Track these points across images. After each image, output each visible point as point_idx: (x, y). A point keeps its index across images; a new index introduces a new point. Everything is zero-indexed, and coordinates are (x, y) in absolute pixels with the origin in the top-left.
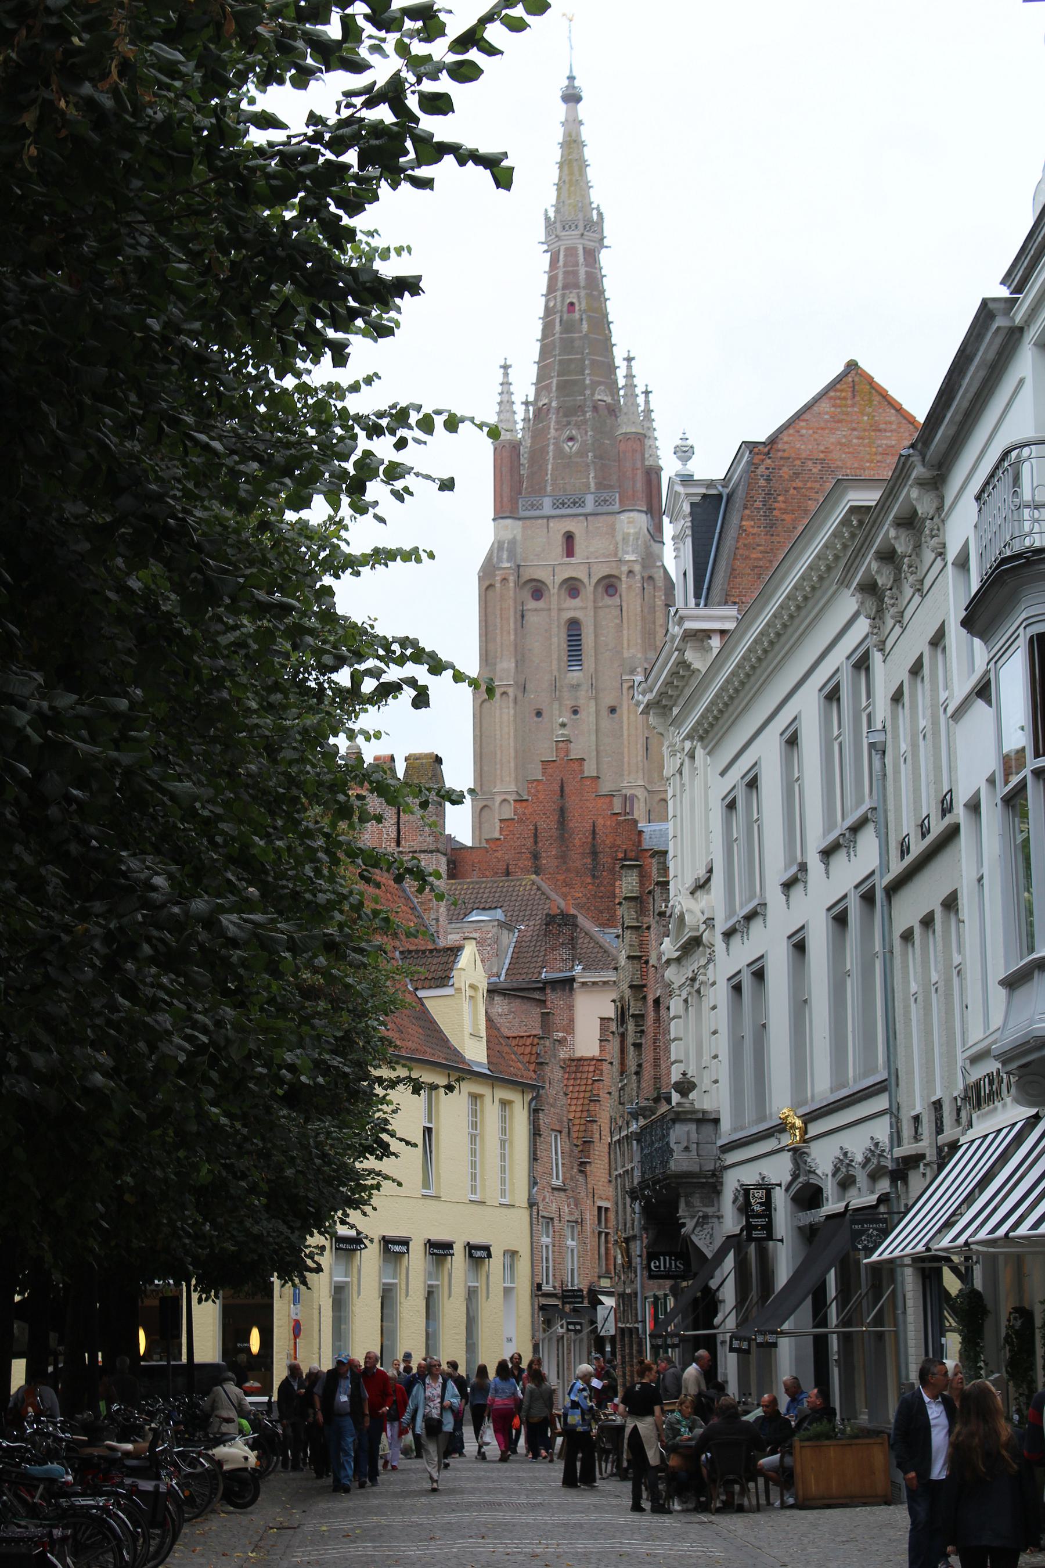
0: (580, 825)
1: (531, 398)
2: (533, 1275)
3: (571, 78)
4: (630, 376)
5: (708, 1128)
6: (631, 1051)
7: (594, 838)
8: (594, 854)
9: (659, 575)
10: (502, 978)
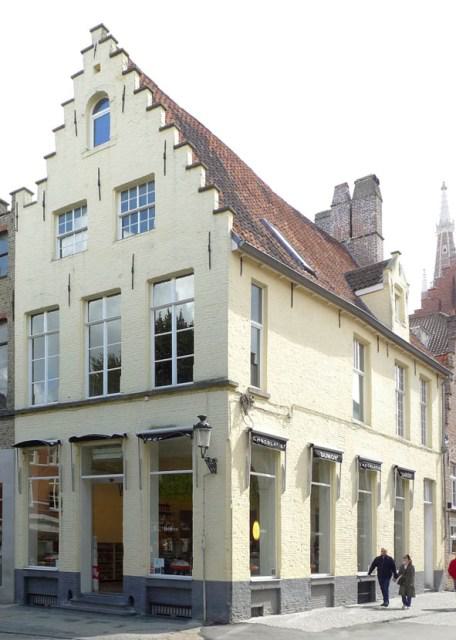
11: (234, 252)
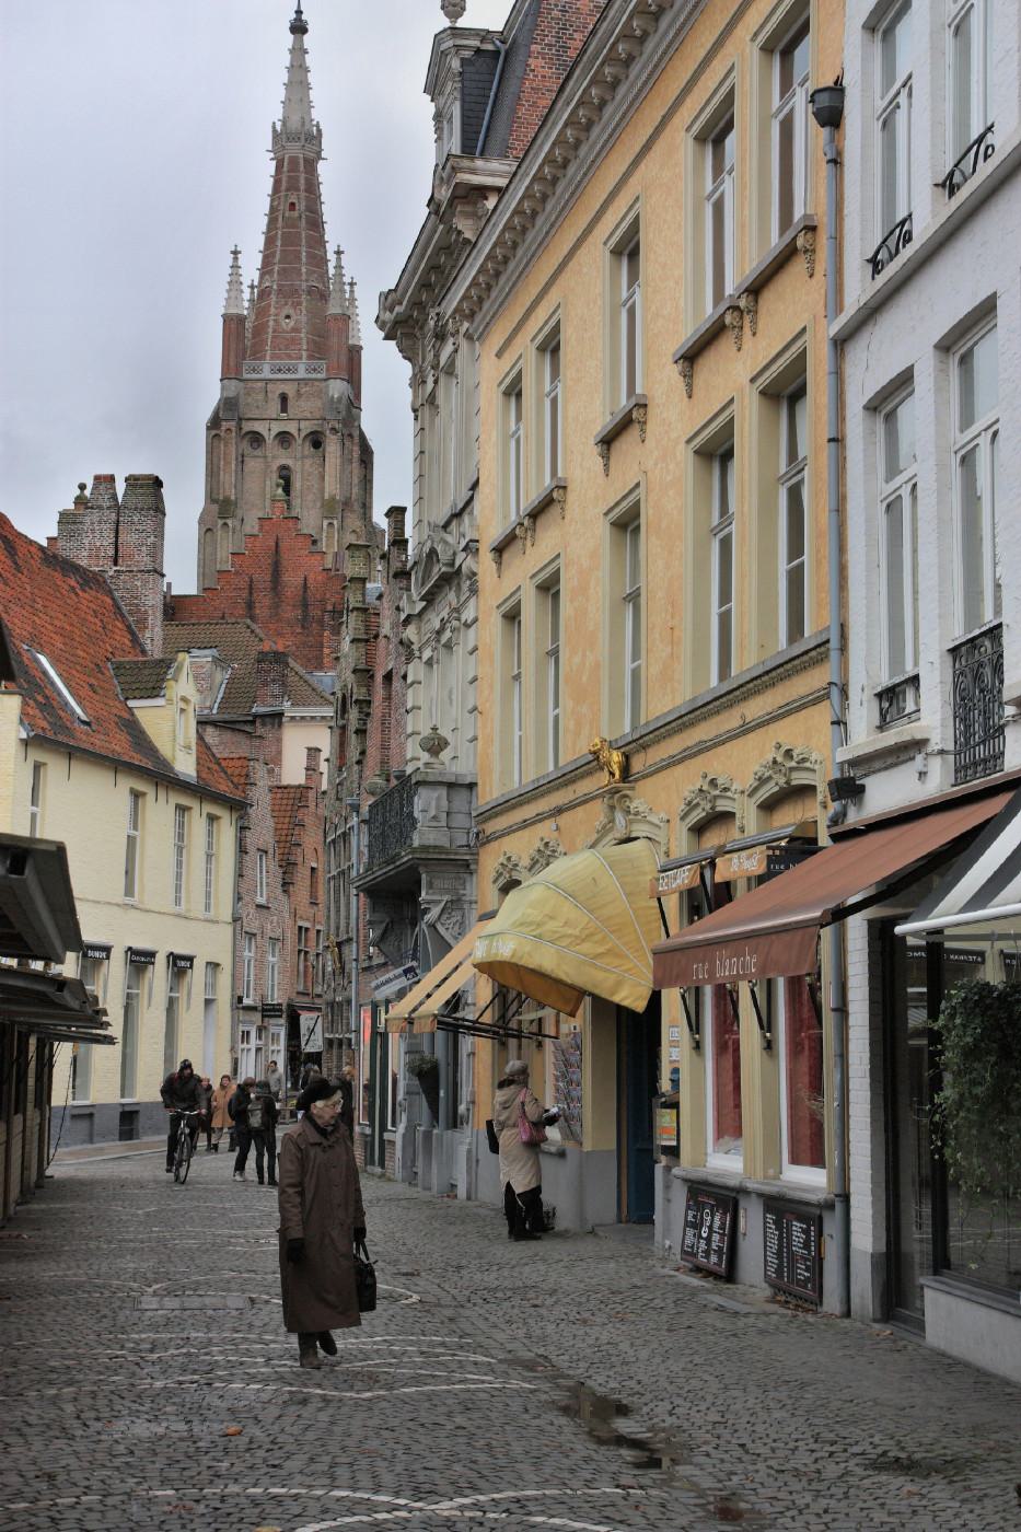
0: (292, 580)
1: (256, 283)
2: (233, 989)
3: (299, 12)
4: (339, 267)
5: (461, 798)
6: (353, 739)
7: (305, 592)
8: (305, 605)
9: (356, 434)
10: (215, 711)
11: (21, 740)
